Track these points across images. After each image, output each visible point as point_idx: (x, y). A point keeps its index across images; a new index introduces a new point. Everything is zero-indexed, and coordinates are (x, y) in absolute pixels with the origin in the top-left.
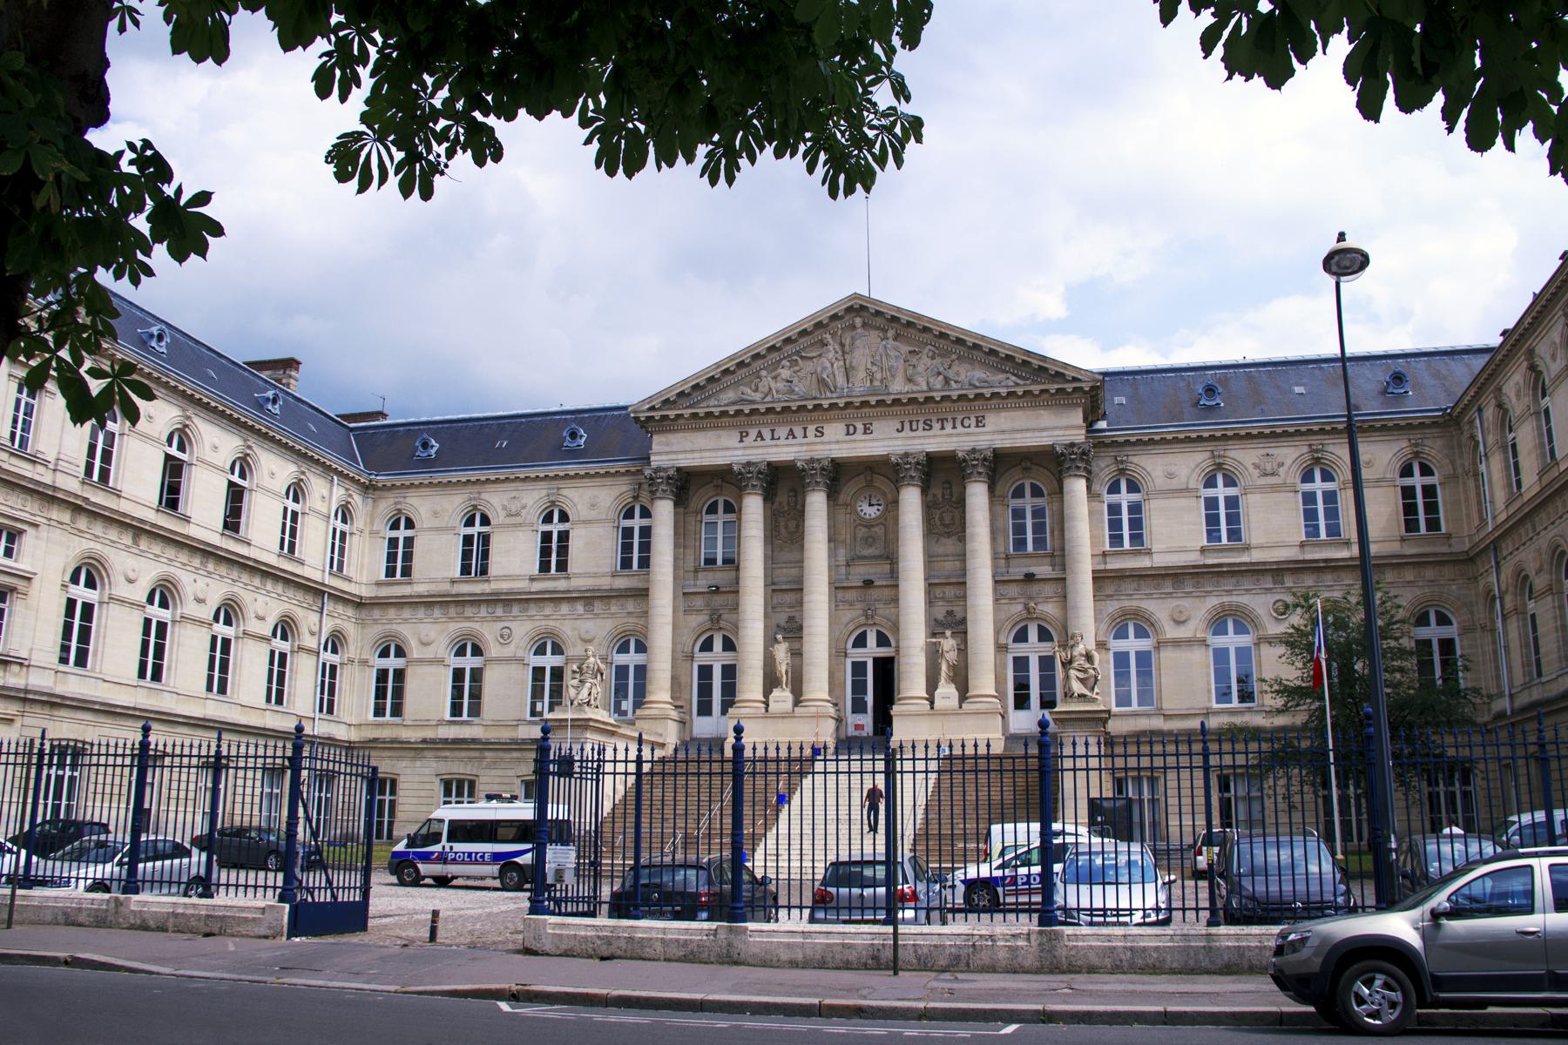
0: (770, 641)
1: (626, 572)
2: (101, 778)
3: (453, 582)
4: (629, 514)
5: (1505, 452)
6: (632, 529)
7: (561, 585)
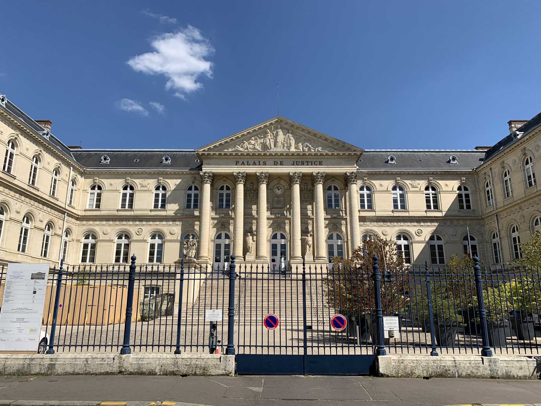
0: (245, 236)
4: (190, 189)
5: (503, 183)
7: (163, 213)
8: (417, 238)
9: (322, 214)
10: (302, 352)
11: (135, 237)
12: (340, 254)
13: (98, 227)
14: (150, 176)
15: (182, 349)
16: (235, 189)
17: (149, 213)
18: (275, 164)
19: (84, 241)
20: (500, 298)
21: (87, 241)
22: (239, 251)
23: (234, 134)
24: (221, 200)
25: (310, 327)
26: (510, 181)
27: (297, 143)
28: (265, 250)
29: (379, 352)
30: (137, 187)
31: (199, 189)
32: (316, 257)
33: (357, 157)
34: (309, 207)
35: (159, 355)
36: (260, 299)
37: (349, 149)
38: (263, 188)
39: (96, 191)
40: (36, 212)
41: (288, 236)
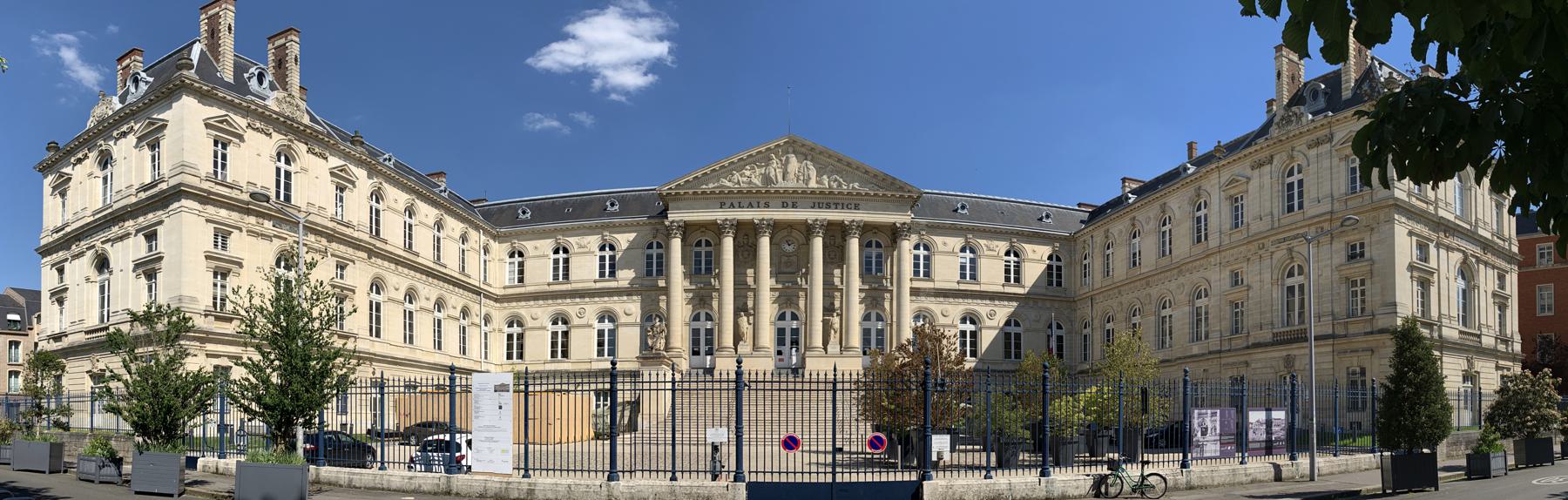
4: (650, 246)
7: (613, 284)
8: (988, 323)
9: (856, 283)
10: (829, 479)
11: (575, 321)
12: (880, 342)
13: (525, 310)
14: (591, 231)
15: (678, 475)
16: (719, 244)
17: (593, 285)
18: (784, 205)
19: (507, 330)
20: (1069, 410)
21: (511, 330)
22: (728, 340)
23: (717, 162)
24: (698, 263)
25: (841, 450)
26: (1116, 255)
27: (819, 175)
28: (767, 337)
29: (924, 477)
30: (574, 249)
31: (664, 246)
32: (844, 348)
33: (912, 201)
34: (837, 272)
35: (651, 482)
36: (761, 408)
37: (901, 188)
38: (765, 243)
39: (517, 259)
40: (447, 296)
41: (802, 316)
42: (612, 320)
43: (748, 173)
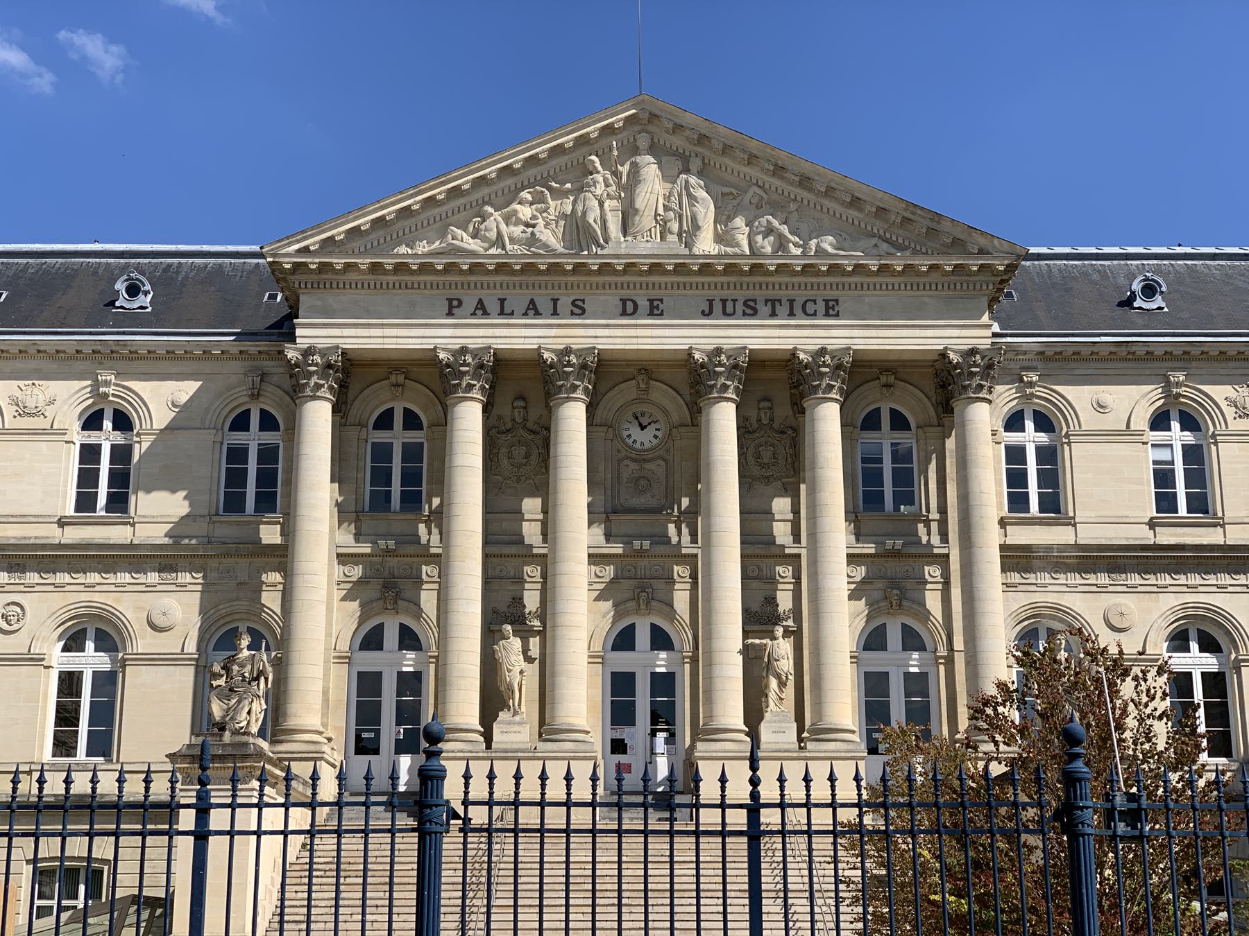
0: (490, 635)
1: (234, 517)
2: (659, 872)
3: (62, 523)
4: (241, 423)
6: (388, 447)
7: (118, 534)
9: (838, 537)
12: (919, 714)
14: (60, 364)
16: (443, 422)
17: (54, 534)
18: (628, 309)
24: (381, 476)
27: (724, 216)
28: (582, 701)
31: (282, 423)
32: (810, 731)
33: (993, 281)
34: (781, 505)
37: (958, 245)
38: (573, 418)
41: (682, 638)
42: (106, 642)
43: (525, 212)
